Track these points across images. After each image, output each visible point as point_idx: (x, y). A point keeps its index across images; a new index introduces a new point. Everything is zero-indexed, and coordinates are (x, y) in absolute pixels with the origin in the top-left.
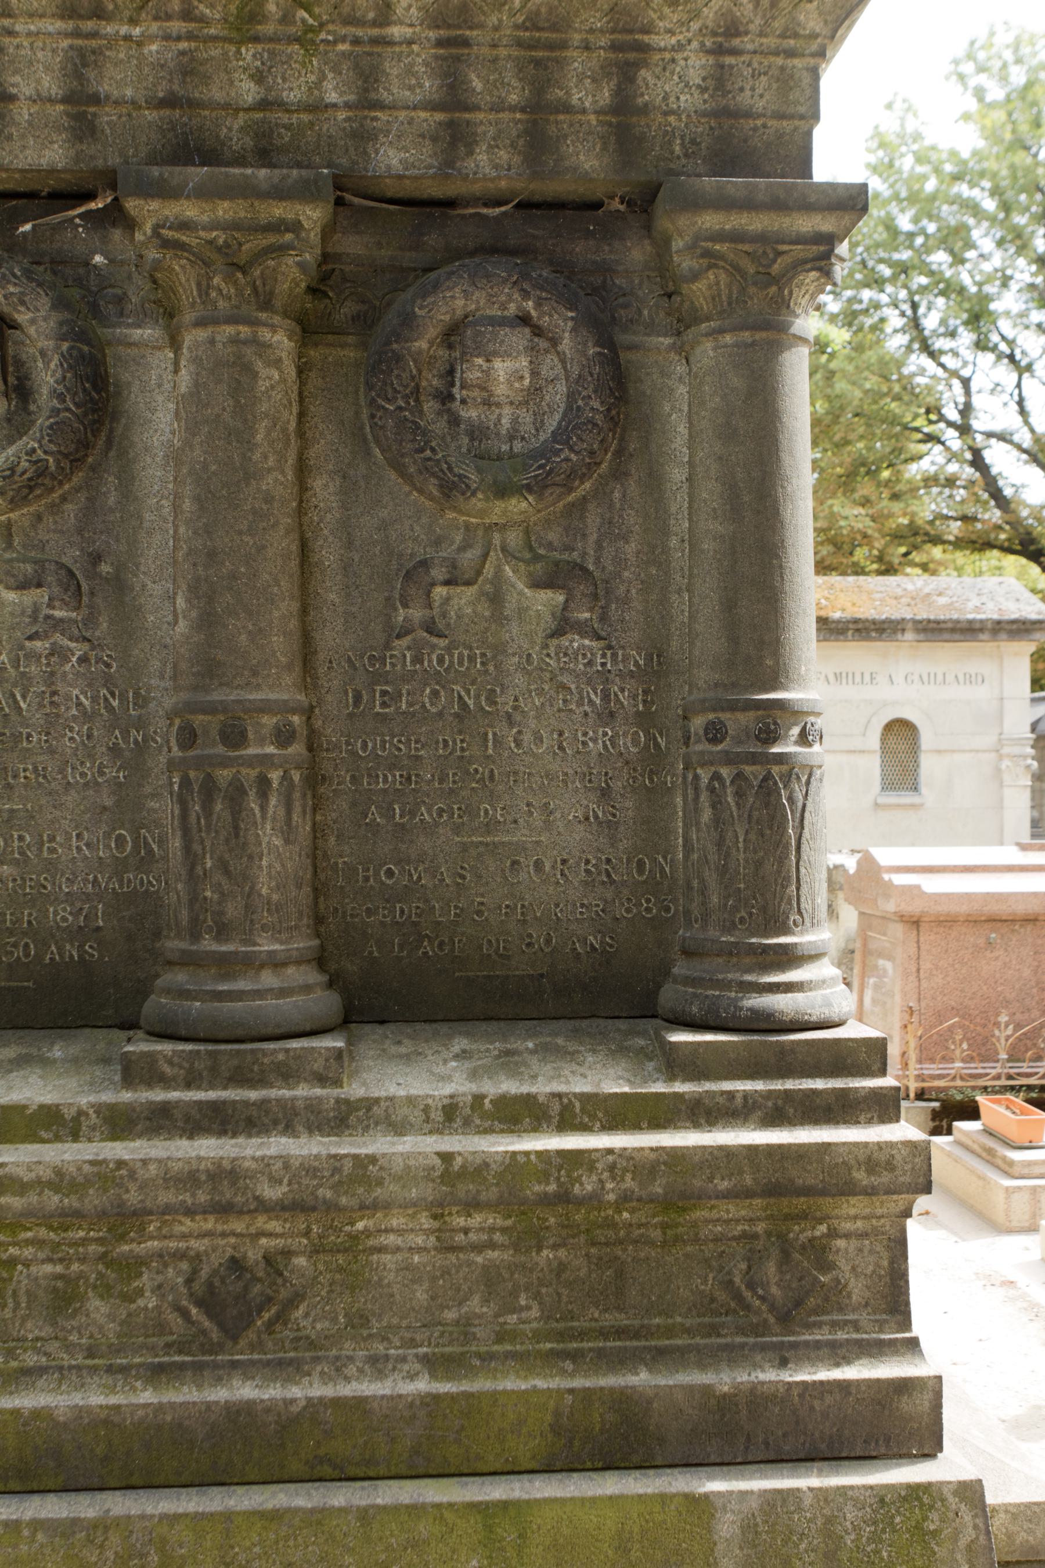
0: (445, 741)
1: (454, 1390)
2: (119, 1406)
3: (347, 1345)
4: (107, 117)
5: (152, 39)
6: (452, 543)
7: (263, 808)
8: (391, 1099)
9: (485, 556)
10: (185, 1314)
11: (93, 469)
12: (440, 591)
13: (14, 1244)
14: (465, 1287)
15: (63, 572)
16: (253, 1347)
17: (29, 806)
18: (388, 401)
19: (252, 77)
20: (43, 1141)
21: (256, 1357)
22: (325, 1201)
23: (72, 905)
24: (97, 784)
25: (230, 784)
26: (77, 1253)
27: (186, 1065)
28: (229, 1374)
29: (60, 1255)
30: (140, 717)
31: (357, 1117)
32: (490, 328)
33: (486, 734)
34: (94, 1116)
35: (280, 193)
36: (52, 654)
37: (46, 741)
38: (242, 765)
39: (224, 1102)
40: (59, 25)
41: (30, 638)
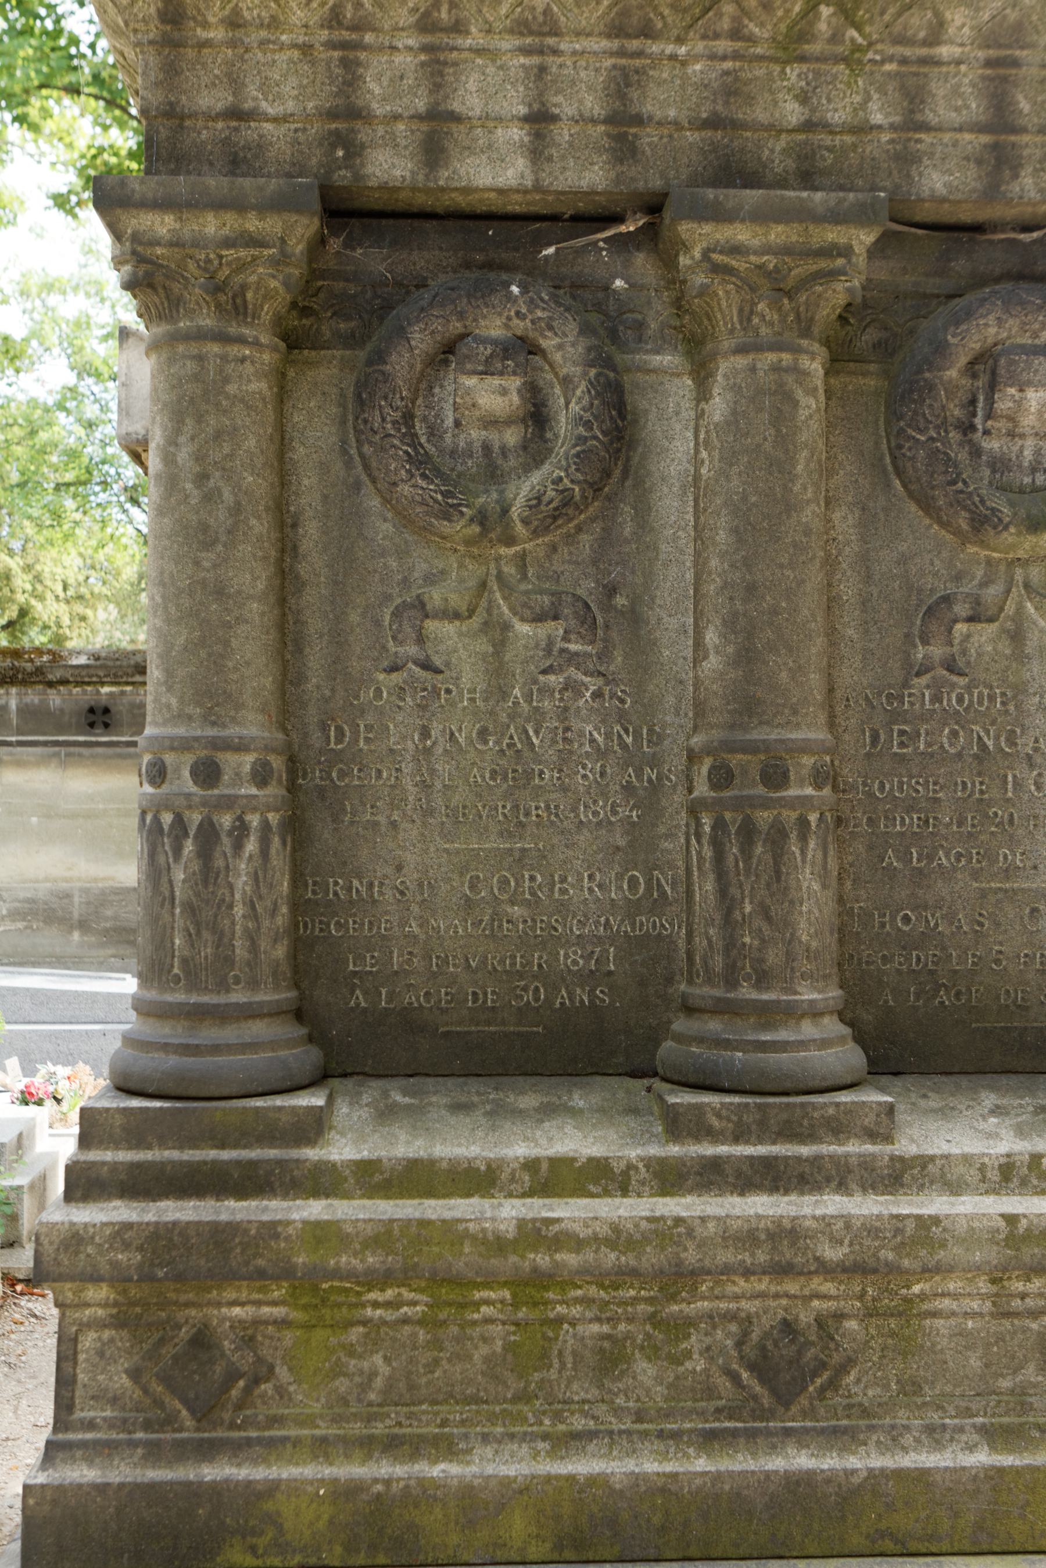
0: (964, 783)
1: (1018, 1463)
2: (677, 1474)
3: (900, 1414)
4: (649, 138)
5: (696, 58)
6: (973, 578)
7: (803, 852)
8: (946, 1157)
9: (1008, 592)
10: (735, 1378)
11: (608, 498)
12: (961, 628)
13: (562, 1302)
14: (1020, 1355)
15: (580, 604)
16: (804, 1414)
17: (541, 846)
18: (921, 431)
19: (796, 97)
20: (592, 1195)
21: (809, 1424)
22: (887, 1264)
23: (583, 948)
24: (611, 823)
25: (772, 827)
26: (626, 1312)
27: (735, 1118)
28: (783, 1442)
29: (608, 1315)
30: (654, 754)
31: (912, 1175)
32: (1024, 357)
33: (1006, 776)
34: (643, 1170)
35: (836, 217)
36: (566, 689)
37: (559, 778)
38: (784, 807)
39: (776, 1158)
40: (605, 44)
41: (544, 672)
